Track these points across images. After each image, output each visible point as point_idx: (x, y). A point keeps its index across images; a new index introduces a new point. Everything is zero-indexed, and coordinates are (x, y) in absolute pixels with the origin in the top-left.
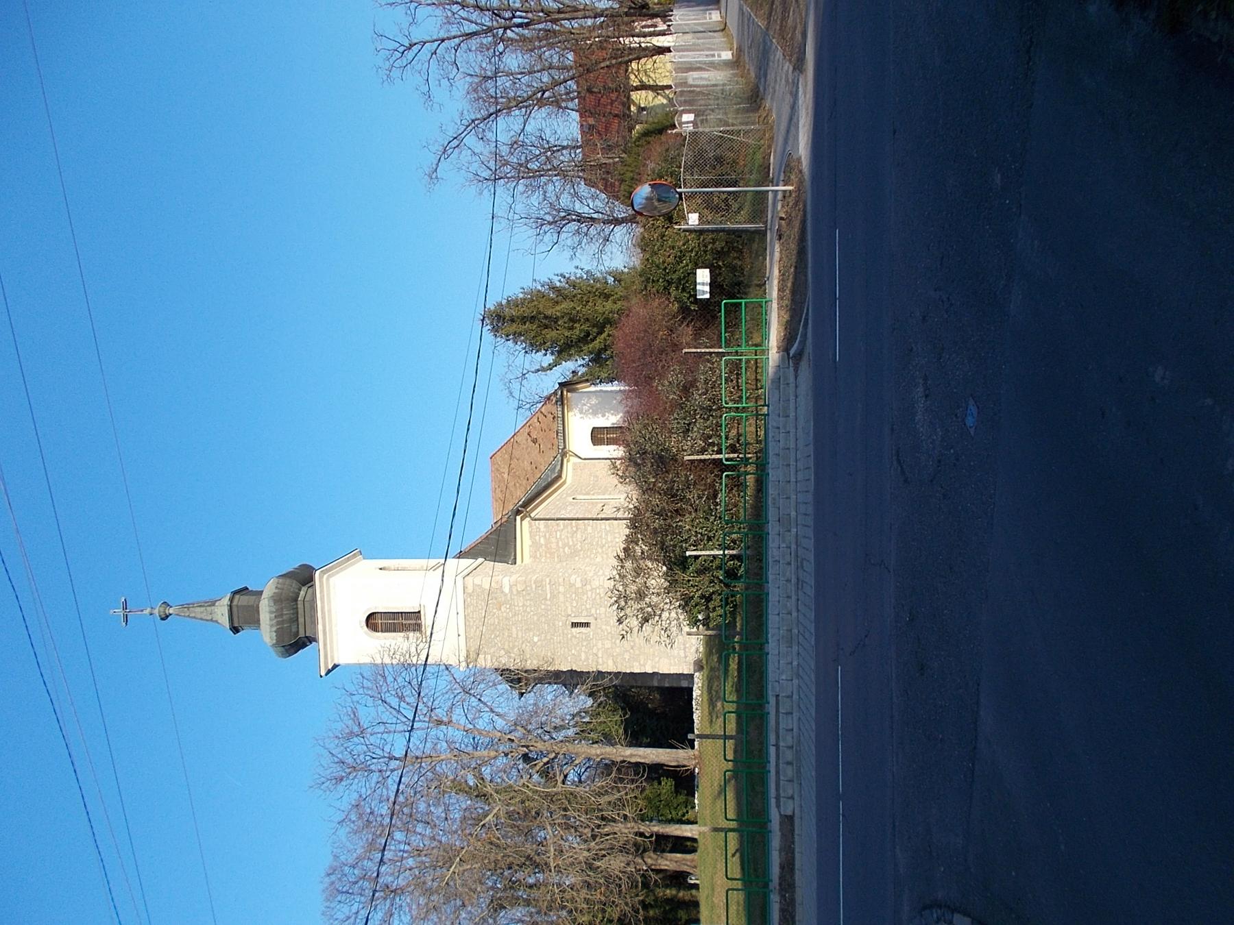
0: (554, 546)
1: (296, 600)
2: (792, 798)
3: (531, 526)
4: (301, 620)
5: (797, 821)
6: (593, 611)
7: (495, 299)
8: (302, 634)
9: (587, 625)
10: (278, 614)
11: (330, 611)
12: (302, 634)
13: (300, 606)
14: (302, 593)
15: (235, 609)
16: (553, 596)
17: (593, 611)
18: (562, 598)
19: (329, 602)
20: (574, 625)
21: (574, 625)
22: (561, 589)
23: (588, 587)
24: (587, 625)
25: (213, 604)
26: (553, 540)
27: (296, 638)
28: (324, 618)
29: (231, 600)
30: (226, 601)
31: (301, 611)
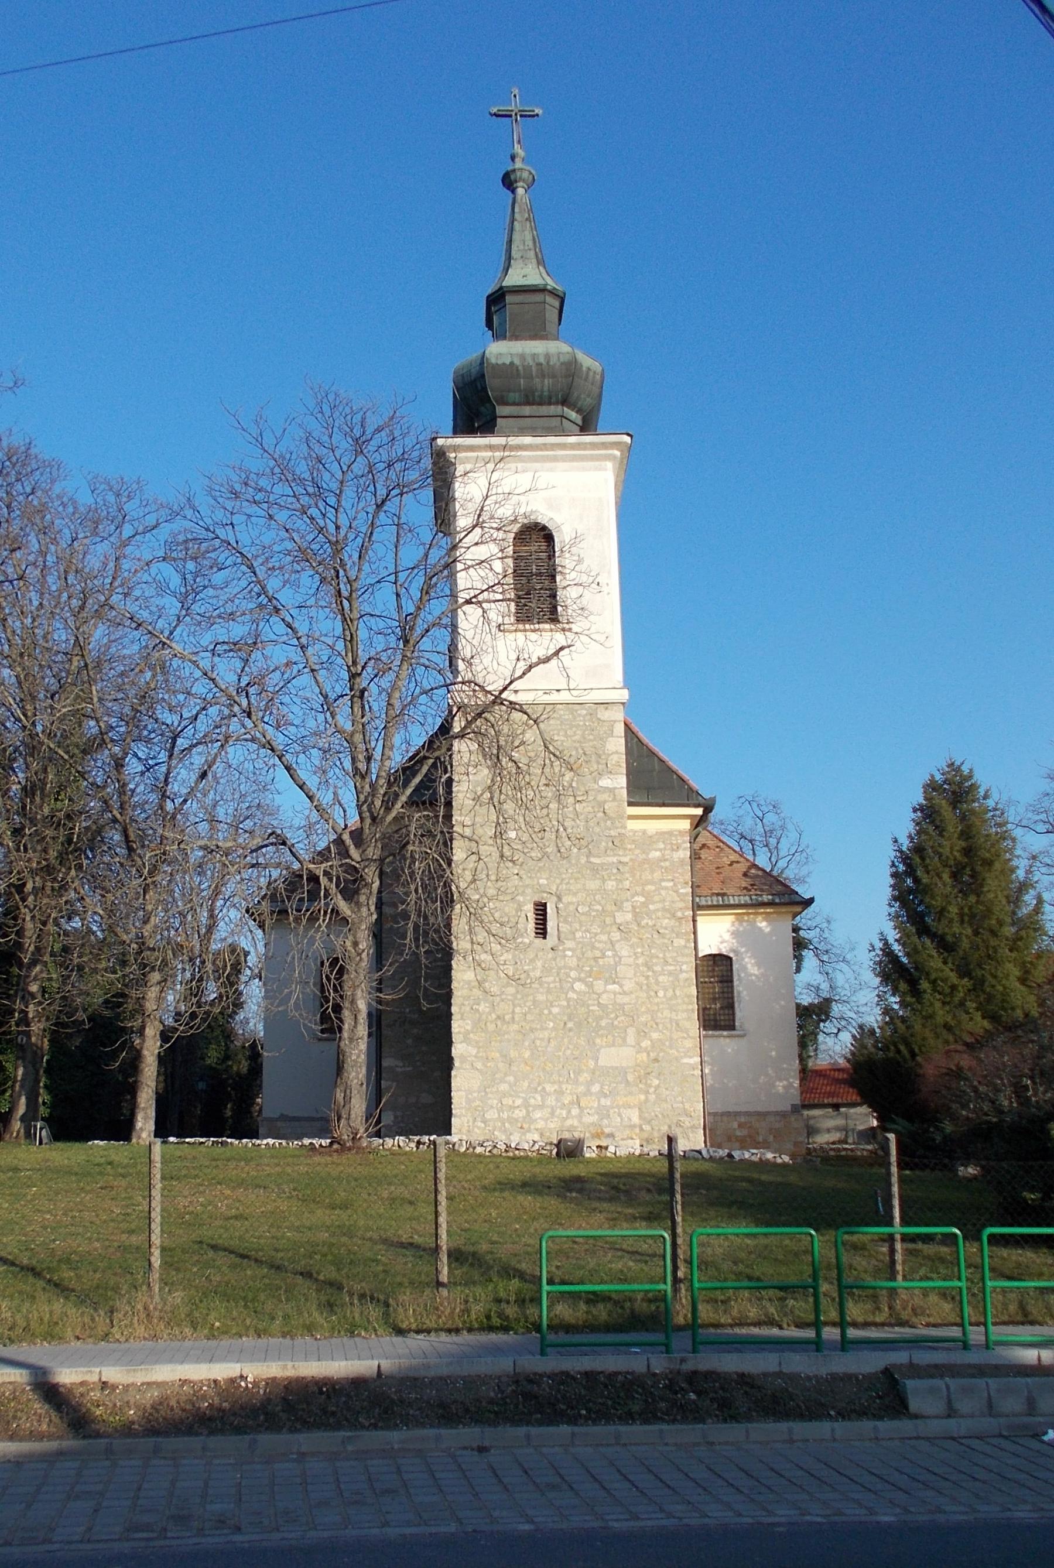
0: (647, 876)
1: (564, 402)
2: (951, 1412)
3: (681, 833)
4: (527, 410)
5: (886, 1426)
6: (569, 944)
7: (984, 778)
8: (501, 410)
9: (542, 931)
10: (544, 369)
11: (555, 459)
12: (501, 410)
13: (554, 409)
14: (573, 415)
15: (538, 297)
16: (595, 870)
17: (569, 944)
18: (593, 885)
19: (574, 459)
20: (541, 910)
21: (541, 910)
22: (611, 885)
23: (616, 936)
24: (542, 931)
25: (541, 262)
26: (657, 875)
27: (478, 406)
28: (544, 447)
29: (553, 293)
30: (551, 283)
31: (544, 410)
